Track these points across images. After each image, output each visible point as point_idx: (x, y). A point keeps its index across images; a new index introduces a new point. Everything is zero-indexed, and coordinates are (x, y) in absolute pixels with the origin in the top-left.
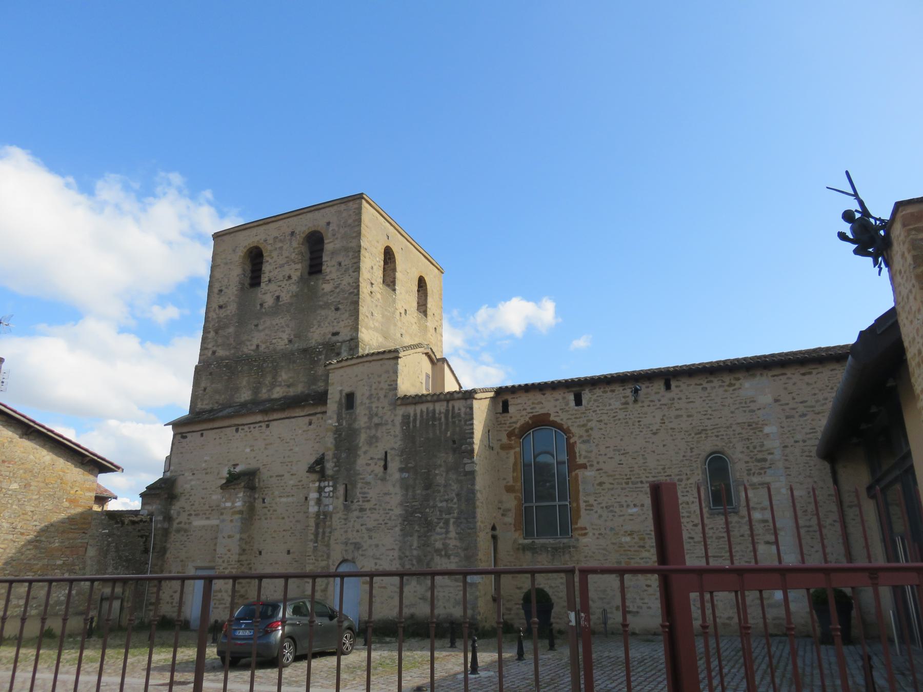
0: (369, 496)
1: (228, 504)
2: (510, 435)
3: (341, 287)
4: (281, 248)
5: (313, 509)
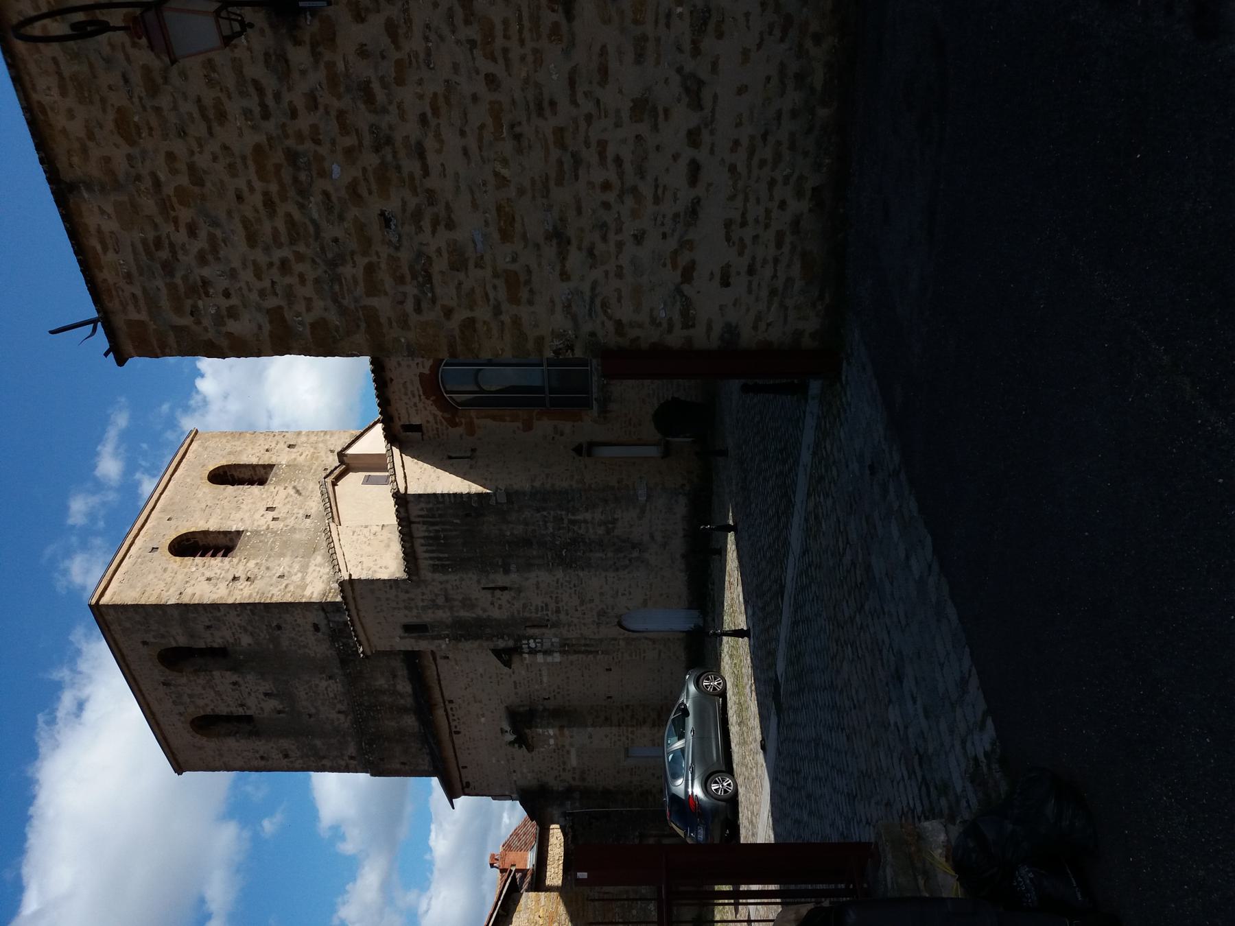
0: (540, 604)
1: (552, 741)
2: (453, 424)
3: (243, 624)
4: (190, 696)
5: (557, 657)
